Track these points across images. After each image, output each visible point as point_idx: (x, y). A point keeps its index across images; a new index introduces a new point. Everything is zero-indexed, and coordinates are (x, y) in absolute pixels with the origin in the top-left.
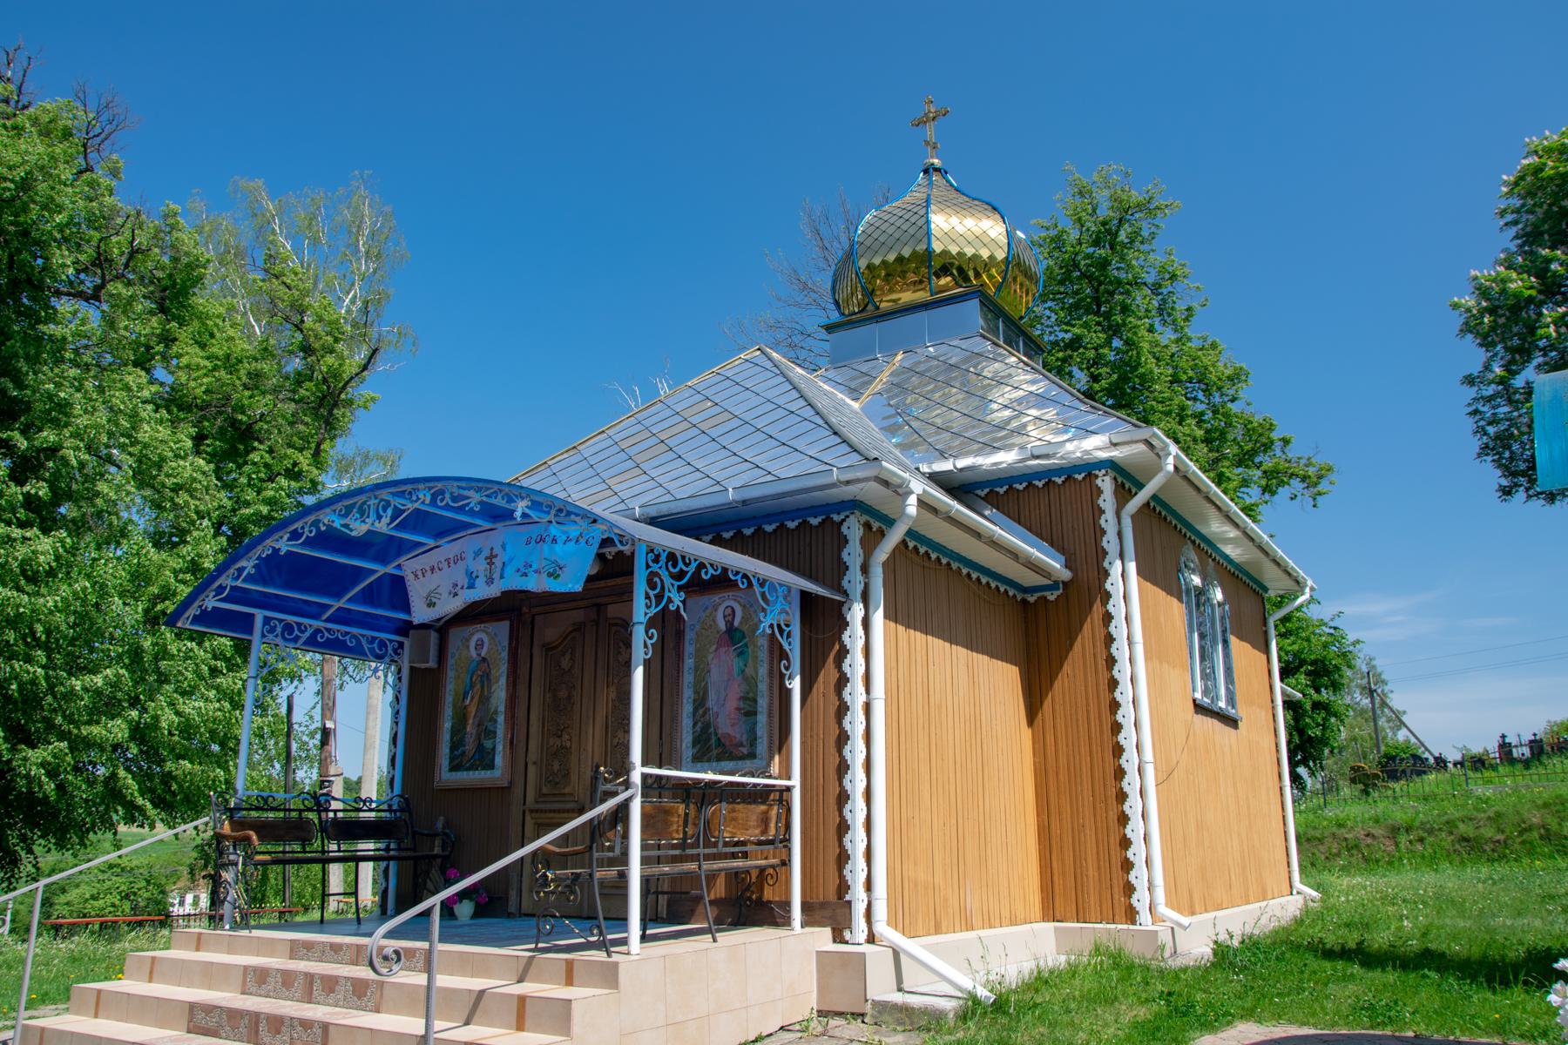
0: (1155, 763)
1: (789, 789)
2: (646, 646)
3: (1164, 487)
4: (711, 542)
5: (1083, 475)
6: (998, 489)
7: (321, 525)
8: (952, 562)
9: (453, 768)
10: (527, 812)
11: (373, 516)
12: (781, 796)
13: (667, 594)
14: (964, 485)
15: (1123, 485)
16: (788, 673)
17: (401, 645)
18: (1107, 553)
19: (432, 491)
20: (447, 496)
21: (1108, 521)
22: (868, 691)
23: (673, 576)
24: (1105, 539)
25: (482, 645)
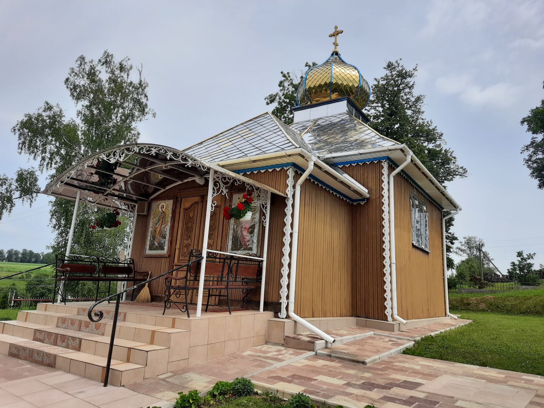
0: (396, 264)
1: (262, 261)
2: (212, 206)
3: (406, 167)
4: (243, 175)
5: (377, 161)
6: (346, 165)
7: (100, 159)
8: (327, 188)
9: (150, 249)
10: (174, 266)
11: (118, 157)
12: (259, 263)
13: (221, 189)
14: (334, 164)
15: (391, 166)
16: (265, 221)
17: (135, 206)
18: (383, 189)
19: (139, 148)
20: (144, 149)
21: (385, 178)
22: (292, 229)
23: (223, 183)
24: (383, 184)
25: (163, 207)
